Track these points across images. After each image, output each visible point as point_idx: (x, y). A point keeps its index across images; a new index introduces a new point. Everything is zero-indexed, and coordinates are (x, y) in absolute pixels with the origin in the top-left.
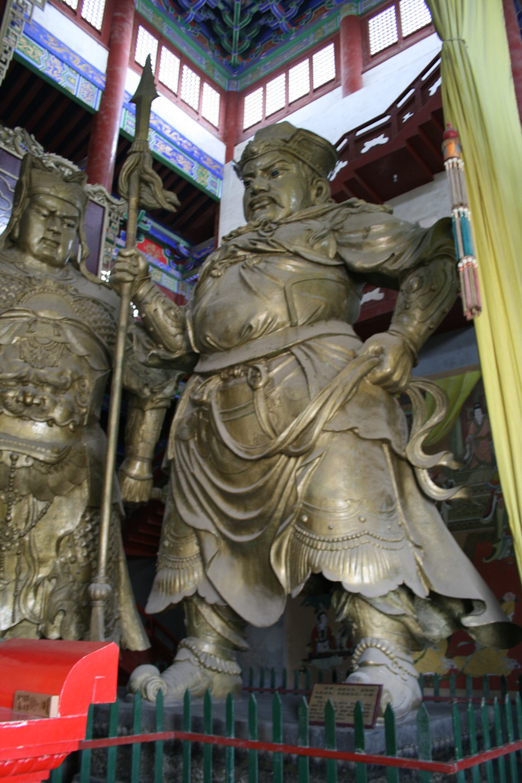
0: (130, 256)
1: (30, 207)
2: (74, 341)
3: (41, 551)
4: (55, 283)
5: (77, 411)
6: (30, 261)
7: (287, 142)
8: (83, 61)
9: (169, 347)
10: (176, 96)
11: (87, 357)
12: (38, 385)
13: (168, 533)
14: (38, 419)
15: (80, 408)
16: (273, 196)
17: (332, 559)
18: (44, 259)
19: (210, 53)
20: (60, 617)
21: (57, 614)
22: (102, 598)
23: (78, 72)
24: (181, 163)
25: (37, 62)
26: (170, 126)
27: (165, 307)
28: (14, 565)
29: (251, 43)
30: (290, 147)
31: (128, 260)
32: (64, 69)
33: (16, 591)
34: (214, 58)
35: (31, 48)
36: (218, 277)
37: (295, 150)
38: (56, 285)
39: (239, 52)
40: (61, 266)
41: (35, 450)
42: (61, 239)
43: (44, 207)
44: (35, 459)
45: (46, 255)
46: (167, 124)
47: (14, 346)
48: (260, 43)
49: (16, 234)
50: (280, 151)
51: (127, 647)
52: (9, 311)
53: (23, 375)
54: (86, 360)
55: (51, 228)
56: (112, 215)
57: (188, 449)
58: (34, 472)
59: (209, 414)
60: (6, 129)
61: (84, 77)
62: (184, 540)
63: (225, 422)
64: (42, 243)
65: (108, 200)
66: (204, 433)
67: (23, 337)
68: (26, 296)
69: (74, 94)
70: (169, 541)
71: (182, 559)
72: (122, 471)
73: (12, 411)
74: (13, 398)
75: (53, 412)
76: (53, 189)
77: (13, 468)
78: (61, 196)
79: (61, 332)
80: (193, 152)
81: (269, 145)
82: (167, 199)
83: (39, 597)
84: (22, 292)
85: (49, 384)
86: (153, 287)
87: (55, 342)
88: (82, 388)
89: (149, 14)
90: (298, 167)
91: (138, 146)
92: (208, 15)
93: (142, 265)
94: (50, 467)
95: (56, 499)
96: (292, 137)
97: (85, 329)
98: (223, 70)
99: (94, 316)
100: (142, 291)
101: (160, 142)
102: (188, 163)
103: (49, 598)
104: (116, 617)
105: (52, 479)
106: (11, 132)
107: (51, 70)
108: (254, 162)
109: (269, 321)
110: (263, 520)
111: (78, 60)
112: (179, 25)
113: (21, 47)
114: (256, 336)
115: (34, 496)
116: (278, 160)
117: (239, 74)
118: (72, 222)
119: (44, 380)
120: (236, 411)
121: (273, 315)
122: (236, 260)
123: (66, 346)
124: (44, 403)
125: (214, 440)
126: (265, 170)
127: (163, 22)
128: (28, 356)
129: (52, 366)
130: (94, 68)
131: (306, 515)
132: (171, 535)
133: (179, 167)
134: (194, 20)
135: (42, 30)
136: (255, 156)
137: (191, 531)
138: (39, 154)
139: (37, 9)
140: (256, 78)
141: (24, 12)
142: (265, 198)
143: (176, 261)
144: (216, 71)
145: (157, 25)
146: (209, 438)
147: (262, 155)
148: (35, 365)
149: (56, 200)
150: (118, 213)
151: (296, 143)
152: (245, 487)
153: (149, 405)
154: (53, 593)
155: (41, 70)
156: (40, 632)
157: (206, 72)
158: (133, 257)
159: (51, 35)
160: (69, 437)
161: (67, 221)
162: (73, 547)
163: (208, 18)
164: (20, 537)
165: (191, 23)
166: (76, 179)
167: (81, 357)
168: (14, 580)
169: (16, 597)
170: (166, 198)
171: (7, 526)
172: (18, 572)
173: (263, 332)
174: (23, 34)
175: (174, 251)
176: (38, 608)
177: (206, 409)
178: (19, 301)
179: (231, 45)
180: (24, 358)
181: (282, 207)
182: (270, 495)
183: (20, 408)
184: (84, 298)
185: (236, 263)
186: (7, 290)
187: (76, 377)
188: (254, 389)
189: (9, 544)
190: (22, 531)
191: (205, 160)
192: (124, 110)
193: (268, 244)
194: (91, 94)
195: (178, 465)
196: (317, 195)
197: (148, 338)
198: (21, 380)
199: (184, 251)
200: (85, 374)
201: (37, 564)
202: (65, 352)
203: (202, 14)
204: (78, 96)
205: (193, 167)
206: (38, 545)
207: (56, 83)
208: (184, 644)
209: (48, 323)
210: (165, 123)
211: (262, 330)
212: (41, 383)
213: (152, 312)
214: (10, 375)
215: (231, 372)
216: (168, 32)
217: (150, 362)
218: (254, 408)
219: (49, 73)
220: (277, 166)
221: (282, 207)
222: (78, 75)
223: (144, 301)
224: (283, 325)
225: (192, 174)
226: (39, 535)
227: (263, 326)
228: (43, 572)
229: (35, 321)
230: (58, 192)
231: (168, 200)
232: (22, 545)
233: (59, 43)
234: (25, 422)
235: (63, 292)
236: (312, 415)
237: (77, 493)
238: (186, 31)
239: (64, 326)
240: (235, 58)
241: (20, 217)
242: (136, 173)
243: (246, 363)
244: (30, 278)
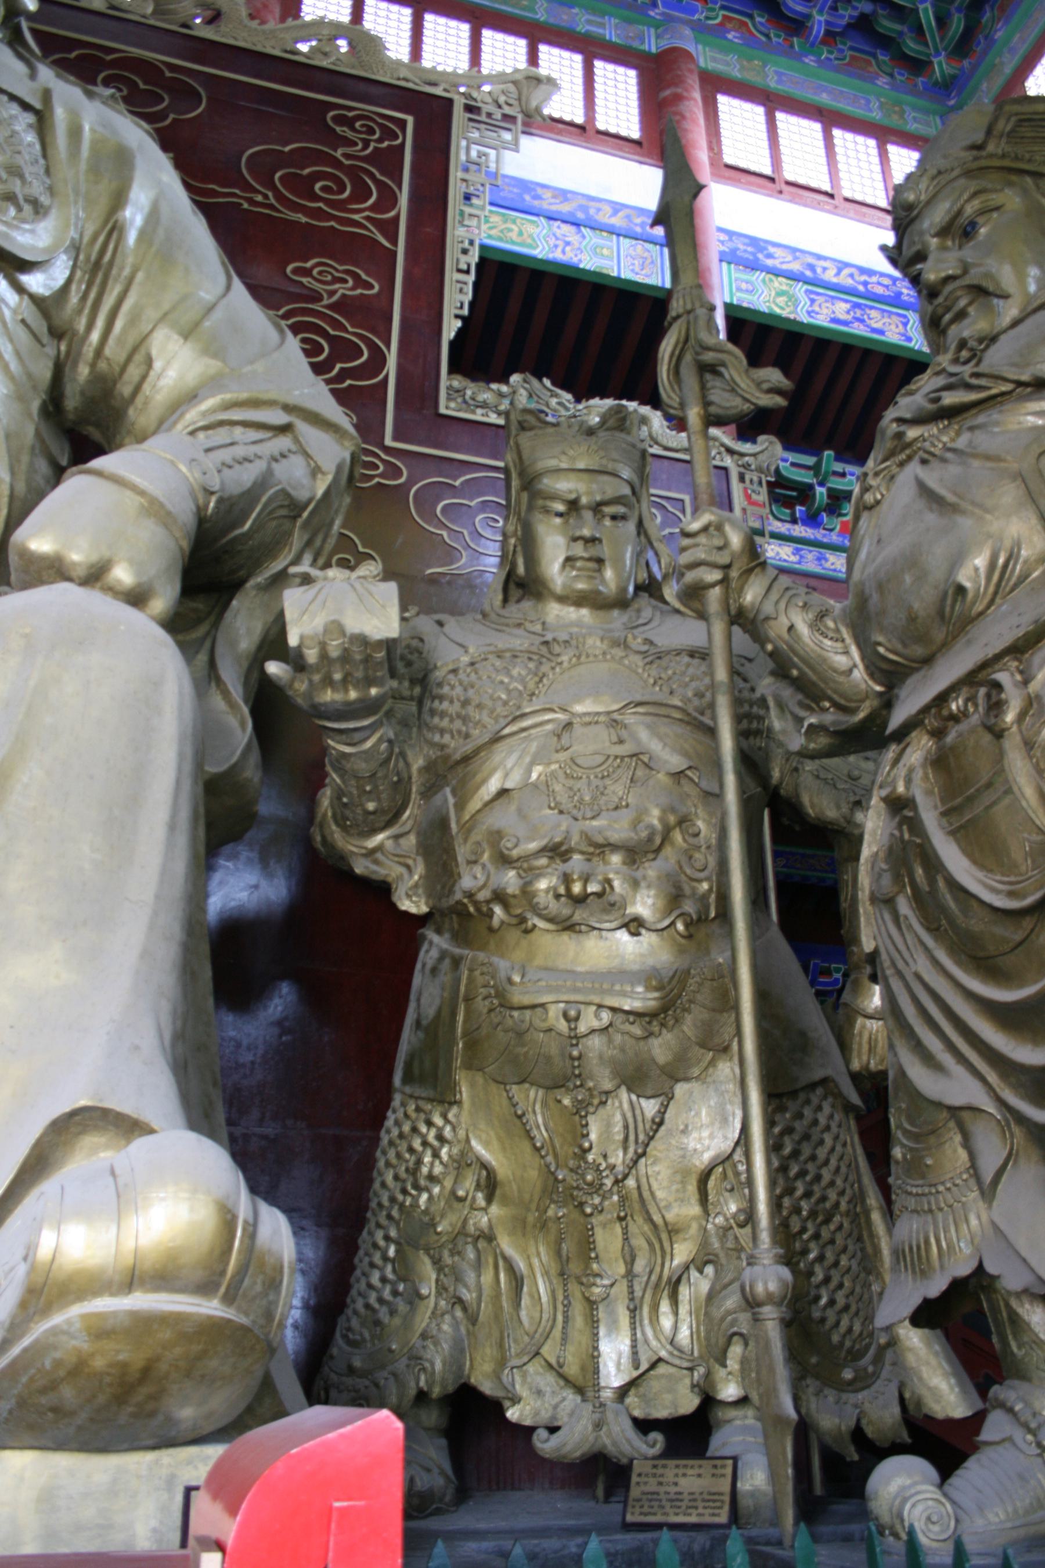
0: (705, 529)
1: (530, 508)
3: (668, 1207)
4: (602, 639)
5: (687, 891)
7: (979, 147)
8: (617, 207)
9: (843, 702)
10: (832, 196)
11: (689, 773)
12: (592, 854)
13: (898, 1127)
14: (607, 925)
15: (695, 884)
16: (975, 282)
17: (631, 1121)
18: (580, 600)
19: (883, 81)
21: (729, 1343)
23: (612, 231)
24: (878, 325)
25: (529, 246)
26: (834, 260)
27: (811, 616)
28: (618, 1242)
29: (967, 17)
30: (991, 156)
31: (702, 539)
32: (584, 237)
33: (632, 1299)
34: (894, 87)
35: (514, 227)
36: (878, 503)
37: (1003, 156)
38: (606, 642)
39: (945, 49)
40: (621, 603)
41: (610, 992)
42: (605, 550)
43: (554, 497)
44: (614, 1010)
45: (581, 591)
46: (825, 258)
47: (535, 786)
48: (987, 8)
49: (521, 569)
50: (968, 174)
51: (925, 1410)
52: (515, 719)
53: (557, 839)
54: (687, 776)
55: (578, 534)
56: (747, 478)
58: (618, 1038)
59: (915, 825)
60: (494, 386)
61: (626, 236)
62: (932, 1140)
63: (953, 833)
64: (568, 569)
65: (730, 451)
66: (919, 872)
67: (549, 764)
68: (545, 680)
69: (615, 274)
70: (903, 1146)
71: (935, 1185)
72: (846, 1005)
73: (550, 920)
74: (547, 891)
75: (634, 903)
76: (564, 458)
77: (575, 1038)
78: (581, 465)
79: (624, 734)
80: (899, 294)
81: (940, 173)
82: (763, 386)
83: (684, 1309)
84: (536, 674)
85: (614, 847)
86: (775, 579)
87: (616, 757)
88: (691, 840)
89: (731, 66)
90: (1025, 192)
91: (681, 302)
92: (855, 8)
93: (736, 540)
94: (649, 1023)
95: (680, 1089)
96: (989, 132)
97: (677, 715)
98: (921, 103)
99: (694, 684)
100: (751, 595)
101: (820, 299)
102: (895, 319)
104: (883, 1341)
105: (661, 1048)
106: (504, 388)
107: (559, 249)
108: (916, 226)
109: (1001, 561)
111: (608, 209)
112: (798, 57)
113: (493, 232)
114: (979, 607)
115: (630, 1090)
116: (965, 197)
117: (959, 94)
118: (621, 509)
119: (600, 840)
120: (971, 799)
121: (1007, 543)
122: (908, 452)
124: (612, 887)
125: (941, 884)
126: (944, 232)
127: (765, 66)
128: (563, 798)
129: (616, 808)
132: (906, 1132)
133: (875, 336)
134: (828, 33)
135: (525, 186)
136: (915, 212)
137: (945, 1114)
138: (567, 409)
139: (508, 155)
141: (484, 169)
142: (959, 293)
144: (907, 109)
145: (752, 77)
146: (932, 882)
147: (928, 203)
148: (580, 816)
149: (572, 475)
150: (760, 470)
151: (1004, 140)
152: (1036, 982)
154: (711, 1296)
155: (540, 257)
156: (698, 1385)
157: (886, 122)
158: (712, 529)
159: (544, 186)
160: (681, 951)
161: (609, 510)
163: (856, 13)
164: (617, 1182)
165: (824, 42)
166: (611, 422)
167: (678, 776)
168: (623, 1277)
169: (634, 1312)
170: (758, 385)
171: (586, 1162)
172: (628, 1258)
173: (996, 593)
174: (488, 208)
176: (684, 1334)
177: (911, 814)
178: (533, 694)
179: (927, 45)
180: (557, 804)
181: (1006, 297)
183: (563, 909)
184: (668, 653)
185: (910, 458)
186: (506, 680)
187: (672, 819)
188: (998, 734)
189: (597, 1200)
190: (620, 1168)
191: (770, 256)
192: (724, 265)
193: (969, 387)
194: (649, 261)
195: (887, 964)
197: (800, 697)
198: (557, 851)
201: (664, 1236)
202: (640, 773)
203: (841, 12)
204: (623, 276)
205: (905, 325)
206: (660, 1194)
207: (577, 269)
208: (996, 1399)
209: (597, 723)
210: (819, 257)
211: (991, 589)
212: (600, 848)
213: (786, 636)
214: (533, 846)
215: (945, 712)
216: (779, 82)
217: (812, 746)
218: (1007, 781)
219: (558, 255)
220: (969, 210)
221: (1006, 297)
222: (614, 237)
223: (762, 617)
225: (909, 339)
226: (658, 1173)
227: (989, 578)
229: (569, 725)
230: (573, 459)
231: (765, 386)
233: (564, 195)
234: (581, 937)
235: (619, 652)
237: (726, 1069)
238: (819, 61)
239: (629, 719)
240: (941, 66)
241: (519, 533)
242: (688, 357)
244: (546, 643)
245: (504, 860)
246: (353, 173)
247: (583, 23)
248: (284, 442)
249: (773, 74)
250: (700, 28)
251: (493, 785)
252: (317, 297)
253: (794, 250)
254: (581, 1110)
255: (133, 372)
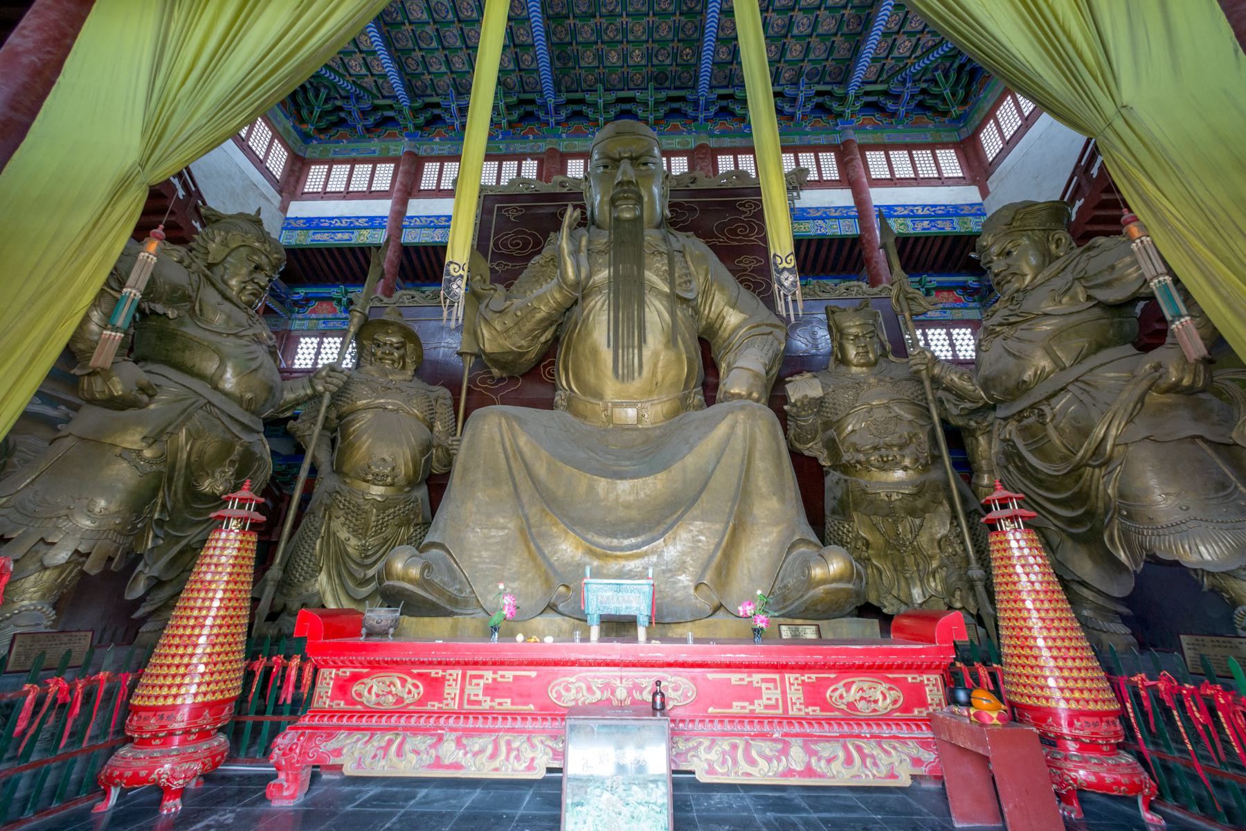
2: (902, 413)
6: (854, 369)
8: (836, 208)
18: (862, 365)
20: (958, 593)
22: (980, 580)
23: (836, 218)
57: (1009, 472)
59: (1014, 446)
95: (927, 515)
100: (936, 371)
103: (945, 581)
105: (919, 503)
110: (1090, 514)
123: (897, 417)
130: (845, 207)
131: (1129, 507)
140: (983, 114)
143: (971, 295)
153: (978, 433)
154: (947, 577)
162: (951, 544)
169: (921, 581)
175: (964, 288)
176: (939, 588)
182: (1088, 496)
196: (1057, 247)
198: (876, 448)
199: (975, 285)
200: (918, 431)
212: (889, 446)
224: (1053, 372)
228: (935, 564)
232: (914, 548)
233: (817, 209)
236: (1101, 435)
237: (941, 509)
243: (1032, 407)
245: (858, 451)
246: (749, 223)
247: (812, 140)
248: (770, 337)
249: (884, 137)
250: (856, 129)
251: (850, 428)
252: (745, 270)
253: (904, 206)
254: (895, 522)
255: (719, 321)
